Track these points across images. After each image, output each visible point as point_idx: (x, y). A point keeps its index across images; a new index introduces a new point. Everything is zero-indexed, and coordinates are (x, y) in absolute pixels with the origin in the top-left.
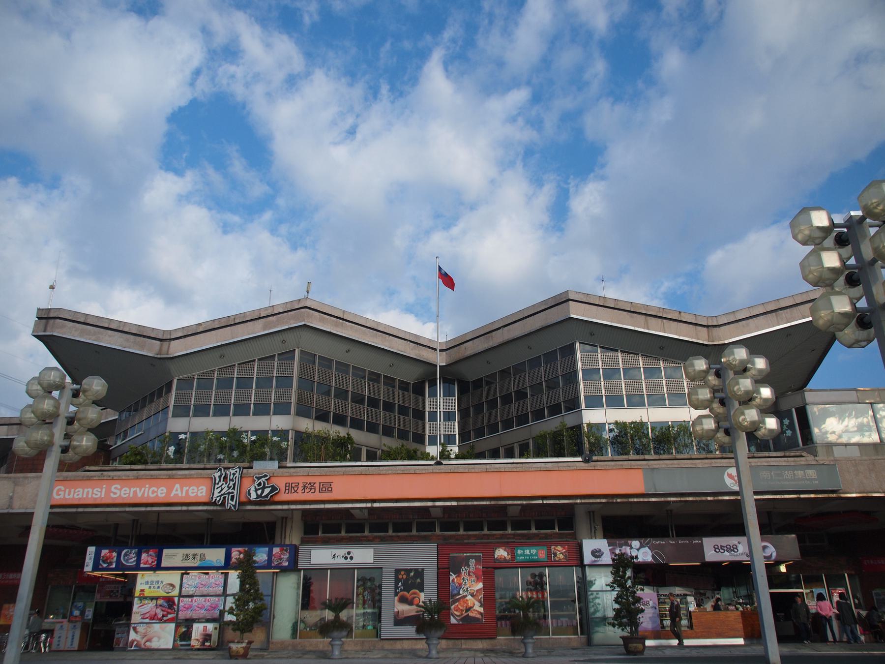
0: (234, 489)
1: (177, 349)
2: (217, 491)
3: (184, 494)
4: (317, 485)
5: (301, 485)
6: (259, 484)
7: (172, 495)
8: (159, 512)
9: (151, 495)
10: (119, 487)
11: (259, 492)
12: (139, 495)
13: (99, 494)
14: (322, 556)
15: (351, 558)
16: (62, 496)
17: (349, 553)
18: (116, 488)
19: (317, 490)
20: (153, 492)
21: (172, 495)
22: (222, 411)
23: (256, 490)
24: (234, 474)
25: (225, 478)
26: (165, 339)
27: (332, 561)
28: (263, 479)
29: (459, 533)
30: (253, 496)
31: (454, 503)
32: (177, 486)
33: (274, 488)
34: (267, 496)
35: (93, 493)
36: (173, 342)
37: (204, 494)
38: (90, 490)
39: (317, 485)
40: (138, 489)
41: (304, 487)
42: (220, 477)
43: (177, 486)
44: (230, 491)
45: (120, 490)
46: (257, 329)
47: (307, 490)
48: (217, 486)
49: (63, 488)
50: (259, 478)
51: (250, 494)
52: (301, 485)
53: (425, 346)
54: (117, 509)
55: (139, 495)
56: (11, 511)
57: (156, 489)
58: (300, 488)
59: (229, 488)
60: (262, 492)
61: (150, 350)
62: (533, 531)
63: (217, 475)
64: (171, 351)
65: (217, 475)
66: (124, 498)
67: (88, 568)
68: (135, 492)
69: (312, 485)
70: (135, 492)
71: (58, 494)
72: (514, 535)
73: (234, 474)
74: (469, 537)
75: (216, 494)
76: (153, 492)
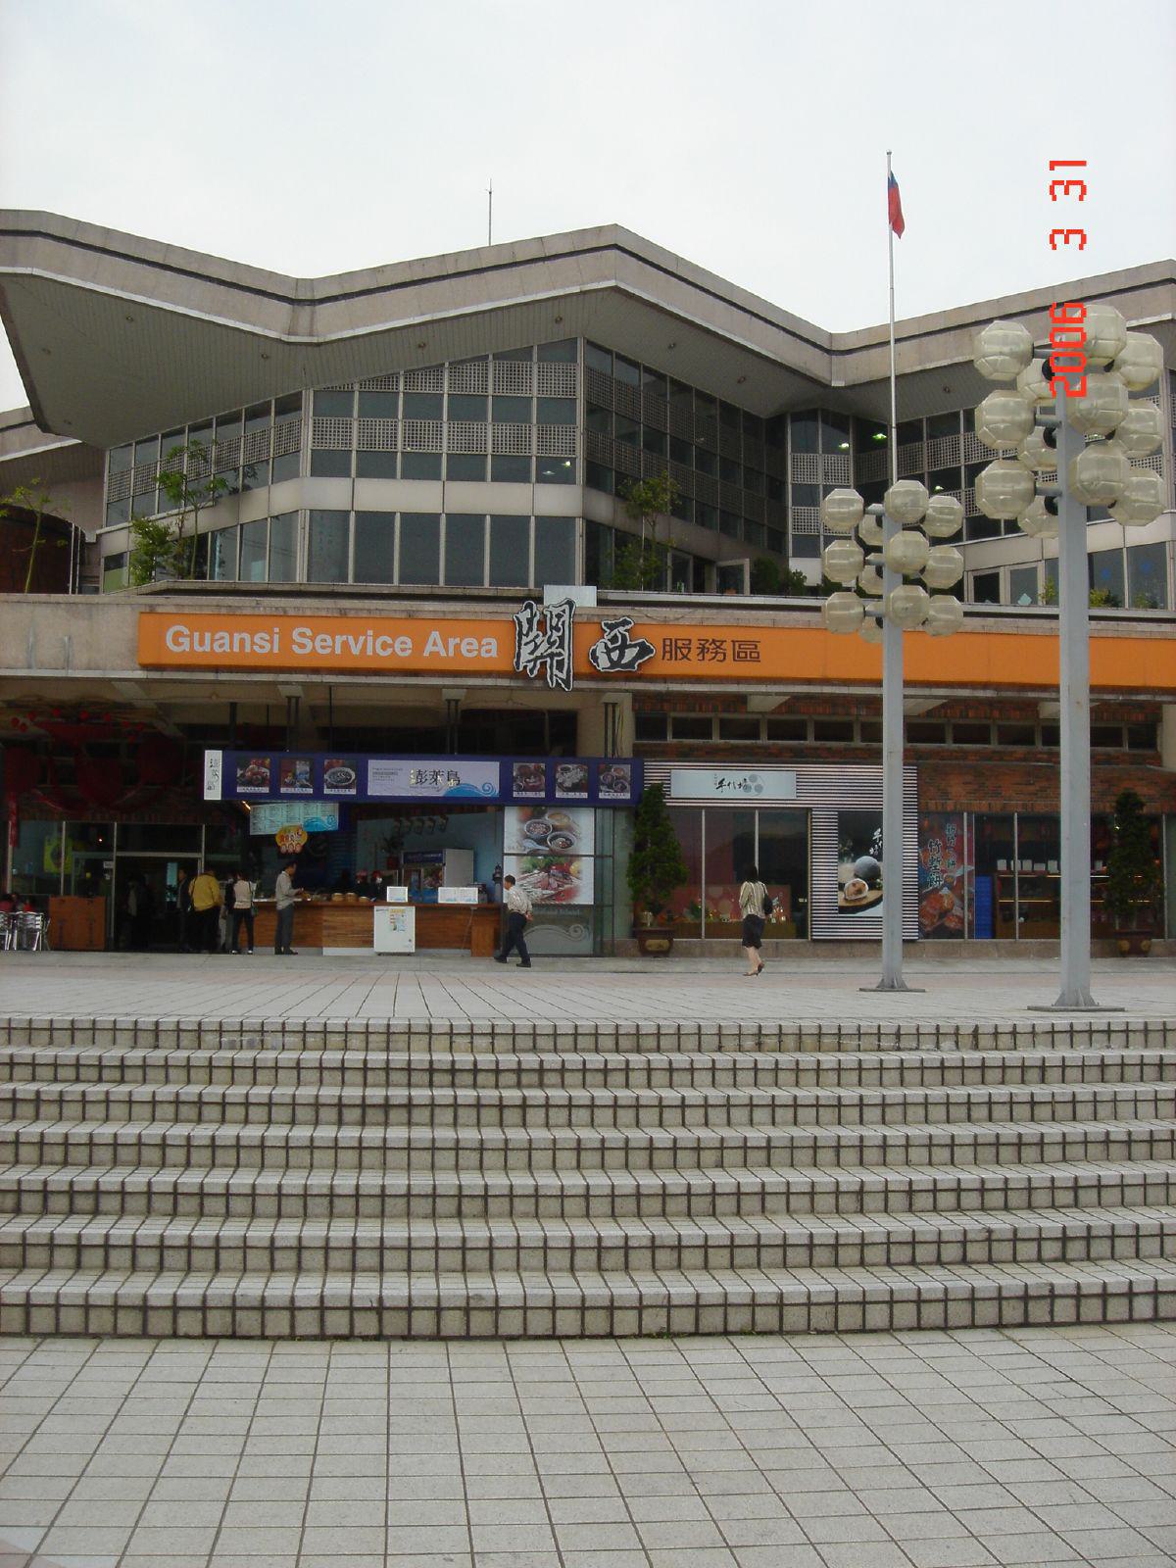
0: (561, 646)
1: (335, 325)
2: (525, 651)
3: (451, 653)
4: (727, 646)
5: (695, 644)
6: (614, 639)
7: (426, 654)
8: (330, 687)
9: (381, 653)
10: (309, 633)
11: (615, 655)
12: (356, 651)
13: (268, 646)
14: (694, 784)
15: (759, 789)
16: (186, 647)
17: (753, 779)
18: (302, 635)
19: (730, 653)
20: (385, 646)
21: (426, 654)
22: (422, 467)
23: (608, 651)
24: (559, 616)
25: (542, 625)
26: (301, 298)
27: (718, 794)
28: (621, 629)
29: (759, 742)
30: (603, 663)
31: (989, 694)
32: (435, 635)
33: (644, 650)
34: (631, 664)
35: (253, 643)
36: (320, 308)
37: (494, 654)
38: (247, 636)
39: (727, 646)
40: (351, 638)
41: (703, 650)
42: (530, 621)
43: (435, 635)
44: (554, 650)
45: (313, 639)
46: (540, 286)
47: (708, 656)
48: (525, 640)
49: (186, 631)
50: (612, 627)
51: (595, 659)
52: (695, 644)
53: (807, 341)
54: (489, 682)
55: (356, 651)
56: (72, 674)
57: (389, 641)
58: (695, 651)
59: (551, 644)
60: (622, 656)
61: (269, 323)
62: (716, 740)
63: (525, 616)
64: (319, 326)
65: (525, 616)
66: (199, 654)
67: (627, 796)
68: (345, 644)
69: (718, 644)
70: (345, 644)
71: (177, 643)
72: (817, 749)
73: (559, 616)
74: (965, 754)
75: (525, 656)
76: (385, 646)
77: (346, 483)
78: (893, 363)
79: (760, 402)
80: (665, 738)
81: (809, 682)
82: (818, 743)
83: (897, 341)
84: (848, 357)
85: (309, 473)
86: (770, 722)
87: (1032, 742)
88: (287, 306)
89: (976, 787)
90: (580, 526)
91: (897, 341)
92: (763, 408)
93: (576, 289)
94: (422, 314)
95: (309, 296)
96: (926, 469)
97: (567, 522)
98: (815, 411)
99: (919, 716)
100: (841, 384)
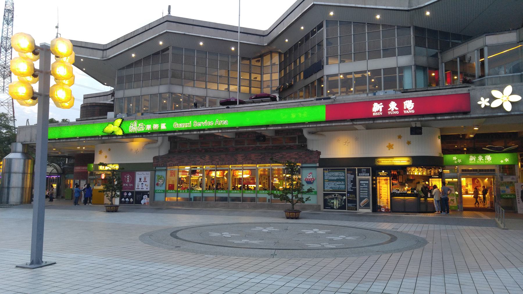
26: (104, 49)
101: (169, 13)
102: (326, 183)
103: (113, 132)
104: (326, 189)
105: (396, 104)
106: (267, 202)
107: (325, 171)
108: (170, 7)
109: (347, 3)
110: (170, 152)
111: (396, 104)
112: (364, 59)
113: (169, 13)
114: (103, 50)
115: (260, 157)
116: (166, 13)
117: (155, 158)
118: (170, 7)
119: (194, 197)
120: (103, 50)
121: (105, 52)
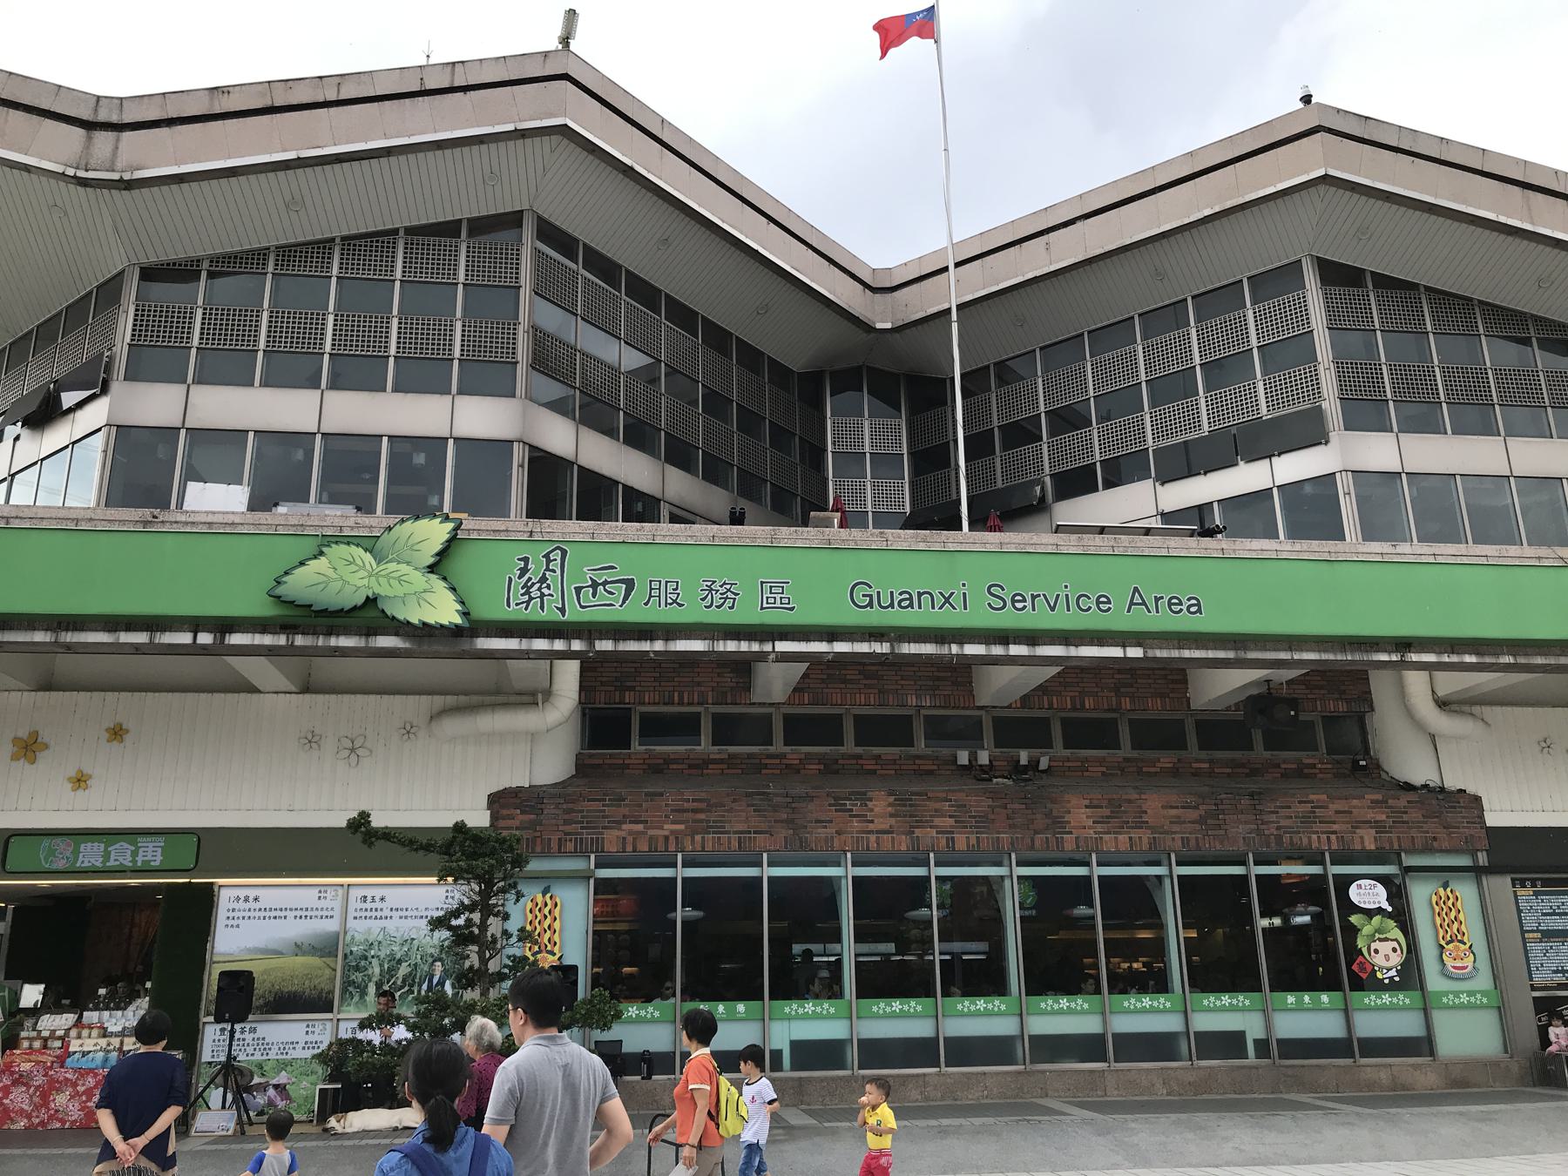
26: (98, 121)
77: (179, 390)
78: (953, 292)
79: (793, 345)
80: (910, 743)
81: (832, 634)
82: (859, 750)
83: (957, 265)
84: (897, 294)
85: (122, 376)
86: (788, 719)
87: (1183, 746)
88: (79, 132)
89: (1106, 812)
90: (519, 455)
91: (957, 265)
92: (796, 359)
93: (510, 127)
94: (285, 150)
95: (114, 119)
96: (996, 423)
97: (501, 447)
98: (857, 371)
99: (1009, 707)
100: (888, 326)
101: (565, 40)
102: (1536, 949)
103: (371, 601)
104: (1538, 978)
105: (626, 1049)
106: (1252, 1059)
107: (1521, 892)
108: (571, 15)
109: (1343, 171)
110: (583, 768)
111: (626, 1049)
112: (439, 387)
113: (565, 40)
114: (89, 126)
115: (1193, 814)
116: (553, 44)
117: (499, 801)
118: (571, 15)
119: (795, 1045)
120: (89, 126)
121: (103, 139)
